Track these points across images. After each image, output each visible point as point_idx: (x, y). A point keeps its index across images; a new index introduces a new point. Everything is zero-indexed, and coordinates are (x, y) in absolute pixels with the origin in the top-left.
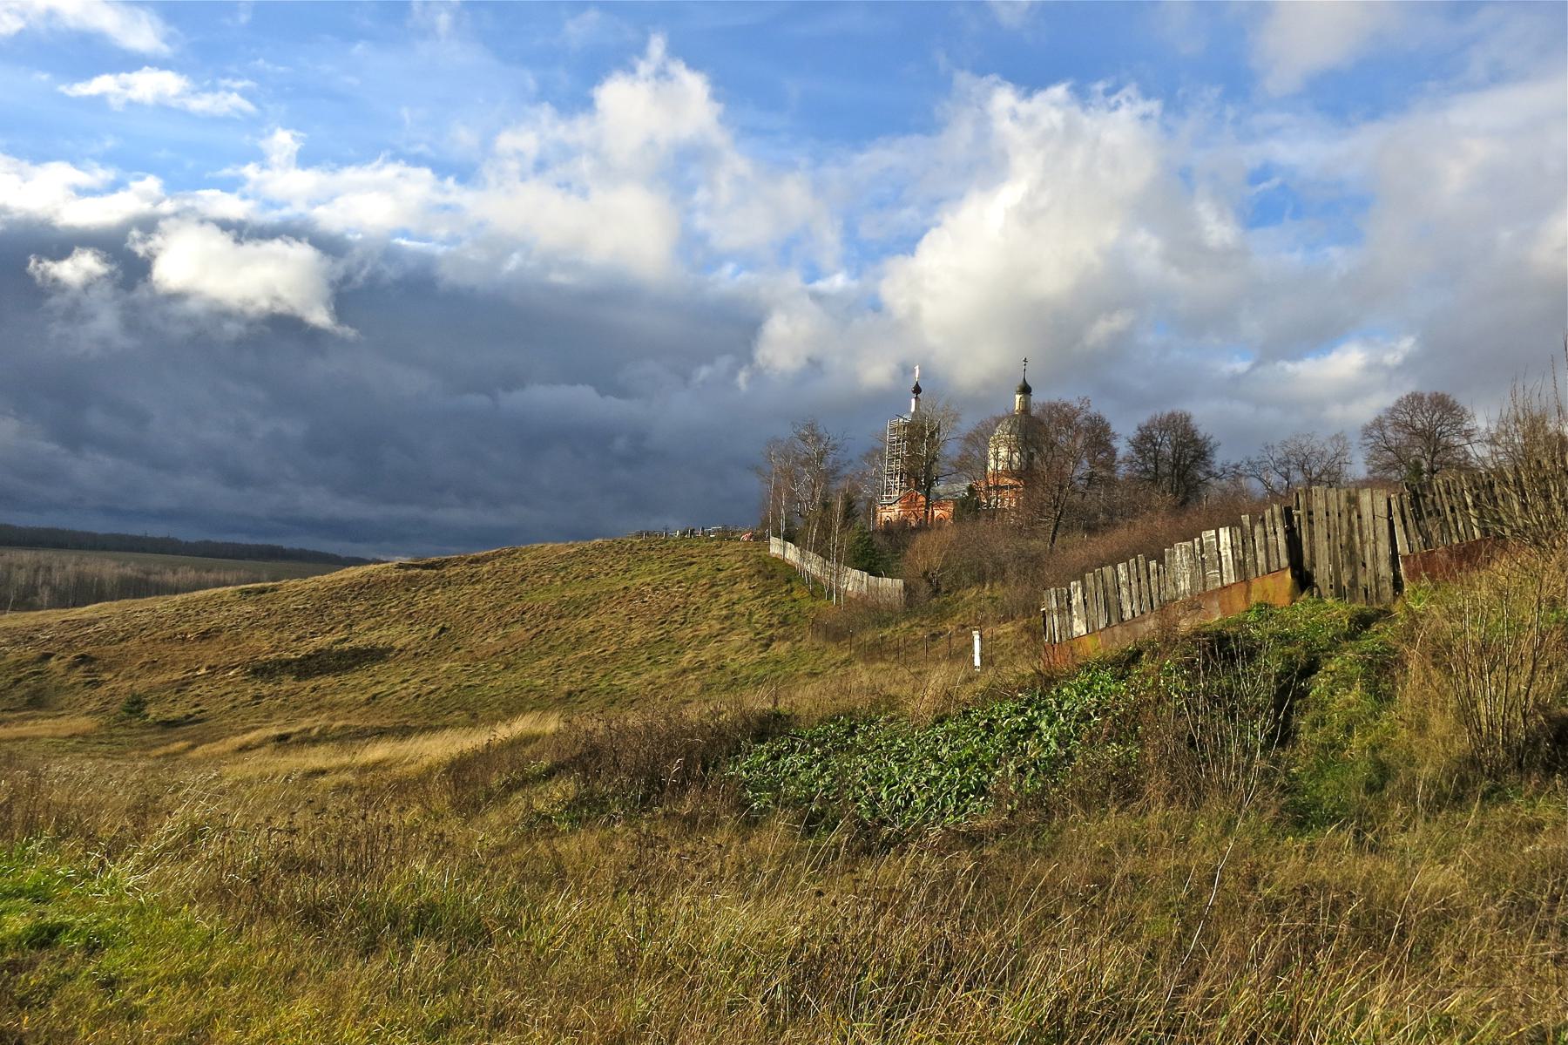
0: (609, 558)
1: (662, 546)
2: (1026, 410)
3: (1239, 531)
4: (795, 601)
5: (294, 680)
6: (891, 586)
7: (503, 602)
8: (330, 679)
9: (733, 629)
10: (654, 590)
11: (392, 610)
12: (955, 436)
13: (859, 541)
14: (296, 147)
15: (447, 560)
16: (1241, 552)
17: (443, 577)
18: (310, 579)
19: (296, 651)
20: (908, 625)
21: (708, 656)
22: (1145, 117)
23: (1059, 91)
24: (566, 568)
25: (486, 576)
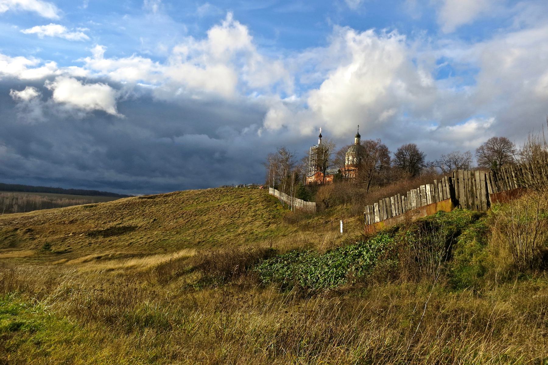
0: (213, 195)
1: (231, 191)
2: (358, 143)
3: (433, 185)
4: (278, 210)
5: (103, 237)
6: (311, 205)
7: (176, 210)
8: (115, 237)
9: (256, 220)
10: (229, 206)
11: (137, 213)
15: (156, 196)
16: (434, 193)
18: (108, 202)
19: (103, 228)
20: (317, 218)
21: (247, 229)
22: (400, 41)
24: (198, 198)
25: (170, 201)
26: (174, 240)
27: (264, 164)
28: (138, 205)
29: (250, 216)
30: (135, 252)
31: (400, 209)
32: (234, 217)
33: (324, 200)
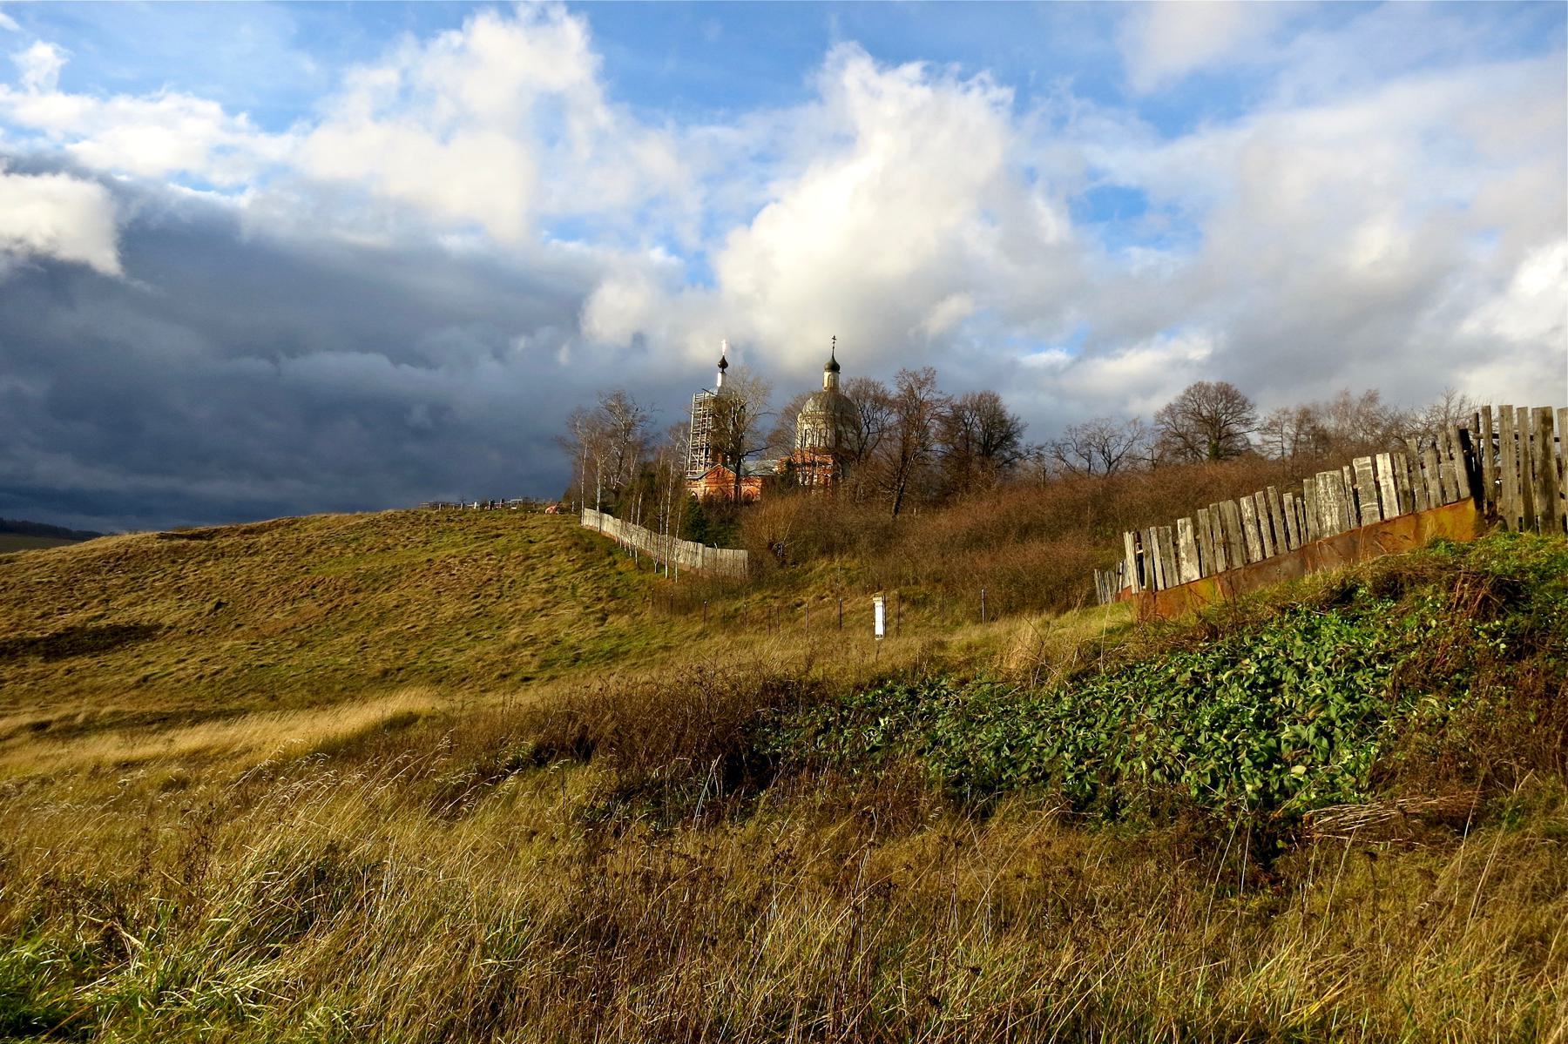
0: (405, 529)
1: (462, 518)
2: (834, 387)
3: (1403, 458)
4: (620, 573)
5: (41, 661)
6: (732, 558)
7: (287, 575)
8: (86, 660)
9: (559, 603)
10: (462, 562)
11: (157, 584)
13: (691, 511)
14: (59, 63)
15: (216, 531)
16: (1406, 481)
17: (214, 548)
18: (52, 550)
19: (42, 630)
20: (760, 597)
21: (537, 631)
22: (996, 104)
23: (913, 70)
24: (356, 539)
25: (265, 547)
26: (297, 667)
27: (561, 442)
28: (160, 557)
29: (538, 593)
30: (169, 707)
31: (1280, 536)
32: (485, 596)
33: (771, 545)
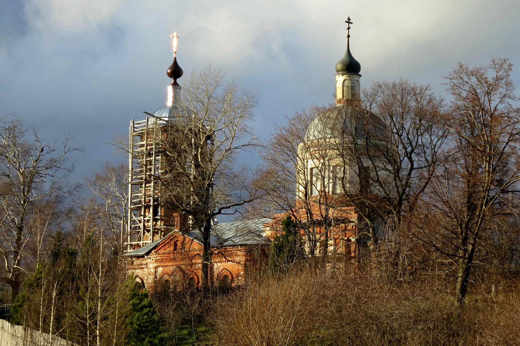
12: (246, 142)
